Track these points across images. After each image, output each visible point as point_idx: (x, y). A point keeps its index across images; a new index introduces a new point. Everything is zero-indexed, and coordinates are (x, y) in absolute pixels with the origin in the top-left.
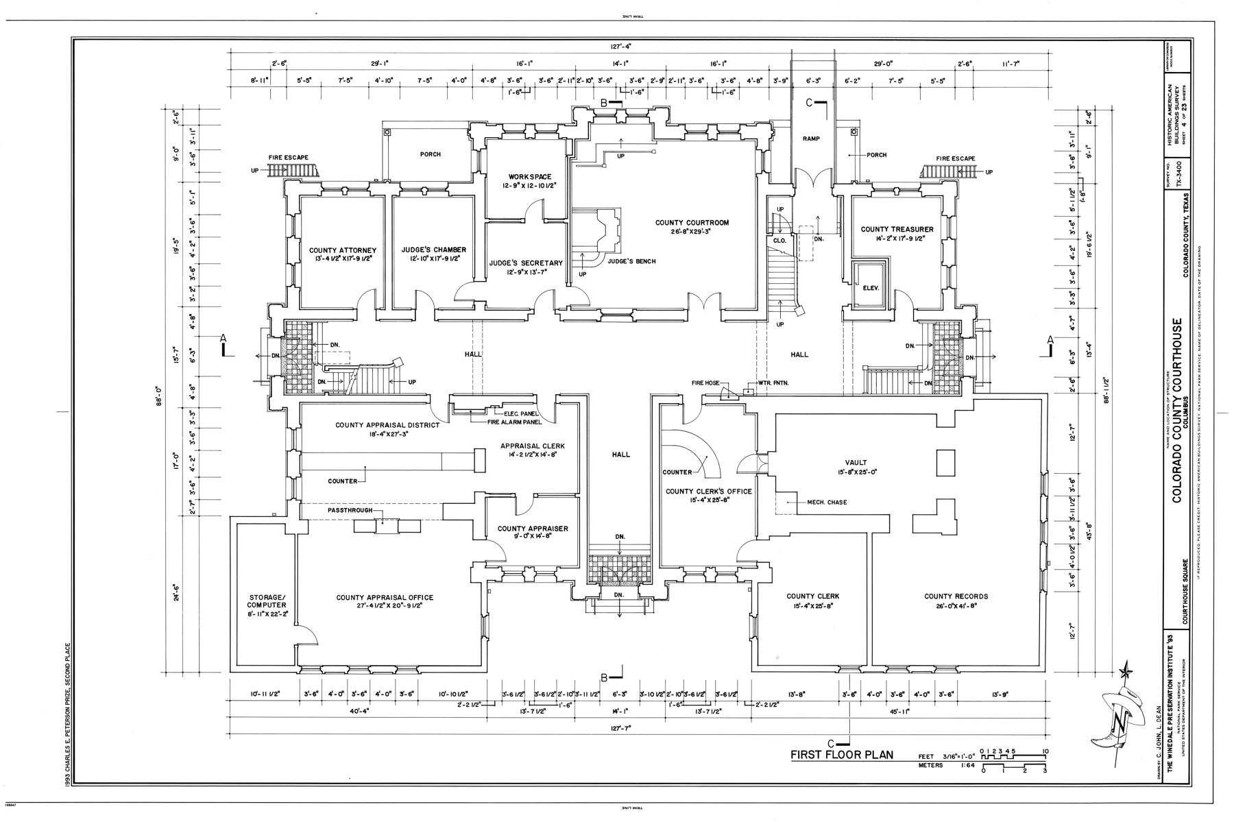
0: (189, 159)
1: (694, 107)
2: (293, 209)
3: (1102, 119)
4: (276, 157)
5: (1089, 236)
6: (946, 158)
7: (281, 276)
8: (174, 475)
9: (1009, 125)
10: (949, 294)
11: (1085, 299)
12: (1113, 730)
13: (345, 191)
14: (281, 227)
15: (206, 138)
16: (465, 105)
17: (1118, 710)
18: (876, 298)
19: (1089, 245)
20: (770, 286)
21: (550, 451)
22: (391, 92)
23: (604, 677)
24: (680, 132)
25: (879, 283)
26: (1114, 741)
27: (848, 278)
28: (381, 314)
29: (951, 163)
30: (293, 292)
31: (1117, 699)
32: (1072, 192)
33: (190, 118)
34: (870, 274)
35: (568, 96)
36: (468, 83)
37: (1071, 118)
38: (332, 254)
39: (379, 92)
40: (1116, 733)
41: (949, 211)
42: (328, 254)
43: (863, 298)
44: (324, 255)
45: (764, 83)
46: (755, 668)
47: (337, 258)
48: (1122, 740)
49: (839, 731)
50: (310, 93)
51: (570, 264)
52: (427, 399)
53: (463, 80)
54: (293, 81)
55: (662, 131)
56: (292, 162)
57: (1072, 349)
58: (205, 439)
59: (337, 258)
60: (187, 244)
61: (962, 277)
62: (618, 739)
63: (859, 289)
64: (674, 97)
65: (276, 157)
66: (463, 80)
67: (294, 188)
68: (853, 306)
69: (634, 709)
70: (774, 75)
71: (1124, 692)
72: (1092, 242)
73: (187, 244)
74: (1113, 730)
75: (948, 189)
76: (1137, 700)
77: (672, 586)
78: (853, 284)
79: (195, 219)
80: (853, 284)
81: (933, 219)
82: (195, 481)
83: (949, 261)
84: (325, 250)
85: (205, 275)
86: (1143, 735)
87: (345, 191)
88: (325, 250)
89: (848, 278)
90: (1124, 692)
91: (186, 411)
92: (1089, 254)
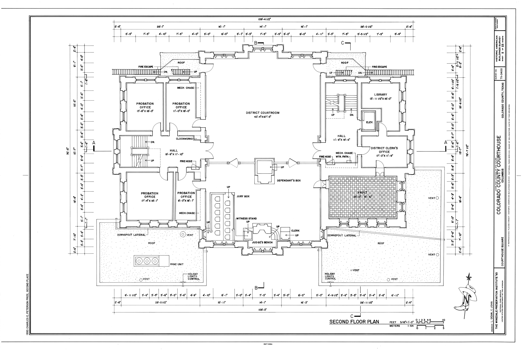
0: (80, 68)
1: (295, 45)
2: (123, 89)
3: (466, 49)
4: (374, 67)
5: (460, 99)
6: (142, 67)
7: (118, 117)
8: (74, 205)
9: (424, 52)
10: (403, 124)
11: (458, 127)
12: (463, 303)
13: (302, 55)
14: (118, 96)
15: (88, 58)
16: (196, 44)
17: (465, 294)
18: (372, 126)
19: (460, 103)
22: (165, 39)
23: (256, 288)
24: (289, 55)
25: (373, 120)
26: (464, 308)
28: (163, 133)
29: (377, 69)
30: (123, 124)
31: (465, 290)
32: (453, 81)
33: (80, 49)
35: (240, 41)
36: (198, 35)
37: (453, 49)
39: (161, 39)
40: (464, 305)
41: (403, 89)
43: (366, 126)
45: (324, 35)
46: (321, 284)
48: (467, 307)
49: (356, 310)
50: (131, 39)
51: (252, 232)
53: (197, 34)
54: (123, 34)
55: (281, 55)
56: (147, 68)
57: (456, 148)
58: (87, 186)
60: (79, 103)
61: (408, 117)
62: (262, 314)
63: (364, 123)
64: (286, 41)
65: (374, 67)
66: (197, 34)
67: (124, 80)
68: (362, 130)
69: (269, 301)
70: (79, 128)
71: (468, 287)
72: (462, 102)
73: (79, 103)
74: (463, 303)
75: (402, 80)
76: (474, 290)
77: (285, 249)
78: (362, 120)
79: (83, 93)
80: (362, 120)
82: (83, 204)
85: (87, 117)
86: (481, 307)
87: (302, 55)
89: (360, 118)
90: (468, 287)
91: (79, 175)
92: (460, 107)
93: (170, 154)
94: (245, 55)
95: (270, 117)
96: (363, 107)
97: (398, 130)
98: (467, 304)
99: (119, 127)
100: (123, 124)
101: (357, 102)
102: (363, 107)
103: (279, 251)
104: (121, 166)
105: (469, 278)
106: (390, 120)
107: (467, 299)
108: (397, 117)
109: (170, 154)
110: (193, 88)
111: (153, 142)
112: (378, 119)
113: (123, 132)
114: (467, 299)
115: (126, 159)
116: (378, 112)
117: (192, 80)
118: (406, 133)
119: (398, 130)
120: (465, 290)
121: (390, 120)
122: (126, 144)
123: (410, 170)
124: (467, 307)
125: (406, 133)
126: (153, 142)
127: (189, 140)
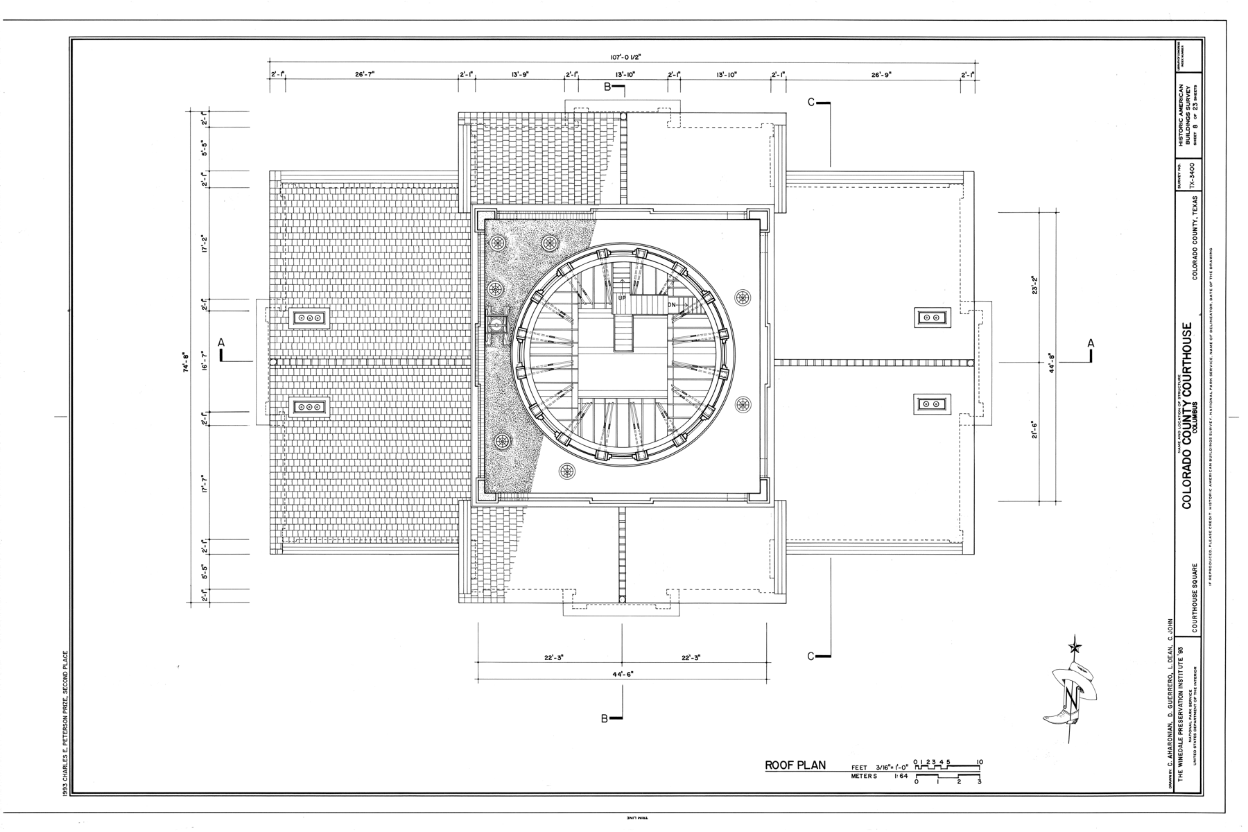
26: (1066, 717)
31: (1068, 675)
40: (1068, 709)
48: (1074, 717)
71: (1074, 667)
90: (1074, 667)
105: (1075, 648)
107: (1072, 697)
114: (1072, 697)
120: (1068, 675)
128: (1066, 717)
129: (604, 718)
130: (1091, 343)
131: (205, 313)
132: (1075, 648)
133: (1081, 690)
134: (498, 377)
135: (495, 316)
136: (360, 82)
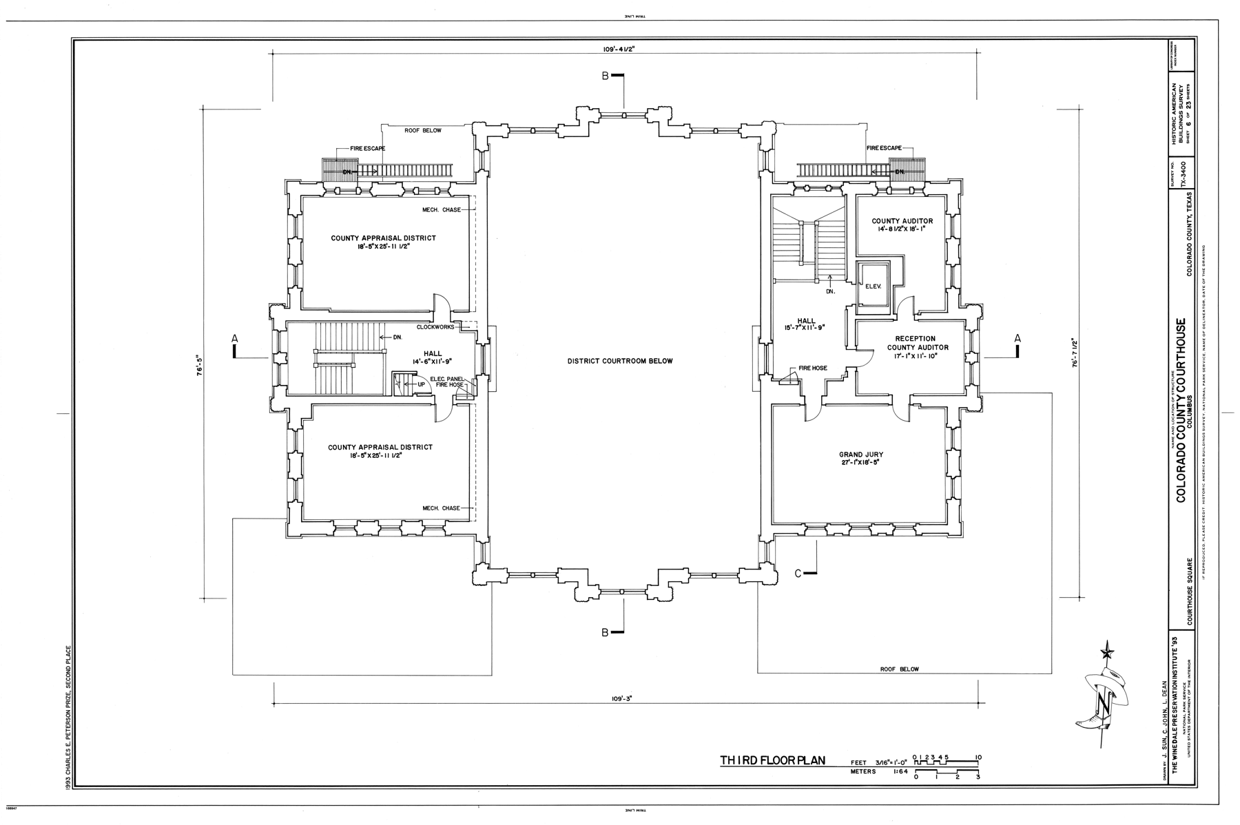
2: (295, 210)
7: (283, 276)
10: (953, 293)
14: (283, 227)
18: (880, 296)
20: (371, 325)
21: (872, 459)
26: (1099, 722)
27: (852, 278)
30: (295, 293)
31: (1099, 680)
34: (874, 274)
38: (895, 225)
40: (1100, 715)
41: (953, 210)
42: (891, 225)
44: (887, 226)
47: (899, 229)
48: (1106, 722)
52: (888, 400)
55: (665, 130)
59: (899, 229)
71: (1107, 673)
76: (1120, 680)
81: (939, 217)
83: (953, 260)
84: (889, 221)
86: (1141, 714)
88: (889, 221)
89: (852, 278)
90: (1107, 673)
93: (426, 362)
94: (583, 130)
95: (932, 356)
96: (860, 253)
97: (306, 518)
98: (1106, 714)
99: (284, 301)
100: (295, 293)
101: (846, 237)
102: (860, 253)
103: (664, 593)
104: (962, 324)
105: (1107, 654)
106: (925, 285)
107: (1104, 703)
108: (939, 277)
109: (426, 362)
110: (458, 210)
111: (399, 337)
112: (897, 279)
113: (294, 313)
114: (1104, 703)
115: (301, 375)
116: (896, 264)
117: (455, 190)
118: (962, 314)
119: (306, 518)
120: (1099, 680)
121: (925, 285)
122: (301, 341)
123: (972, 401)
124: (1106, 722)
125: (962, 314)
126: (399, 337)
127: (445, 330)
128: (1099, 722)
129: (605, 632)
130: (1018, 338)
131: (495, 160)
132: (1107, 654)
133: (1114, 695)
134: (357, 160)
135: (353, 358)
136: (618, 707)
